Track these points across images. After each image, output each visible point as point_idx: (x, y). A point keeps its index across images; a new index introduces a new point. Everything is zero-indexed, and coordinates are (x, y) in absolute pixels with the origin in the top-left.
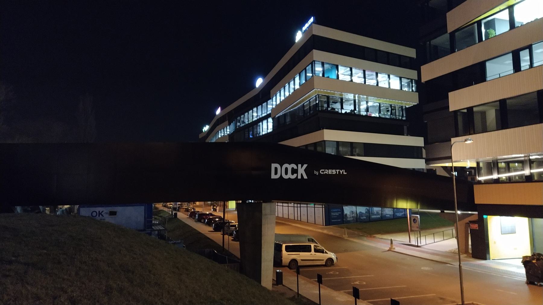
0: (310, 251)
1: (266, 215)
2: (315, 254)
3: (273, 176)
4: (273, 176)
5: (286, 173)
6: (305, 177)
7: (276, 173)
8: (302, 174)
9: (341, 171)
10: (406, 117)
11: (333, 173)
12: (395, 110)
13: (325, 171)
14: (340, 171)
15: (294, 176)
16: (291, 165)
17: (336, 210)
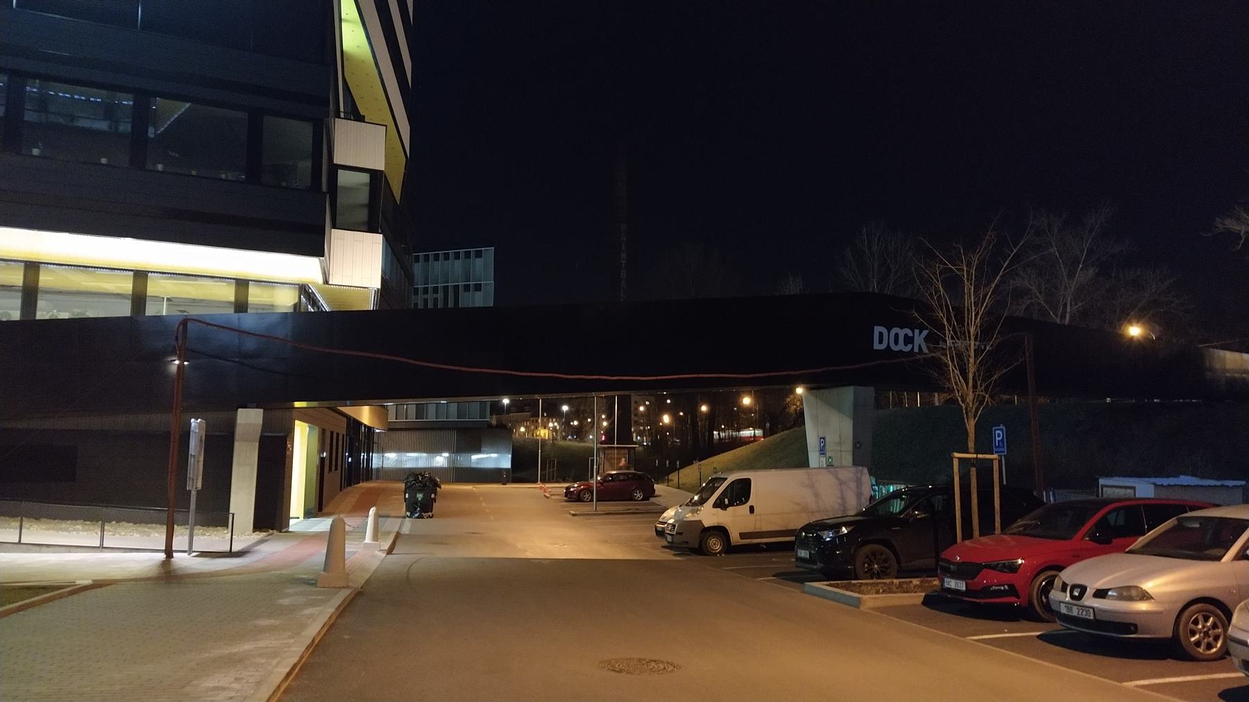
1: (9, 524)
3: (877, 346)
4: (877, 346)
5: (896, 343)
7: (881, 342)
8: (920, 346)
10: (952, 458)
12: (1061, 604)
16: (904, 330)
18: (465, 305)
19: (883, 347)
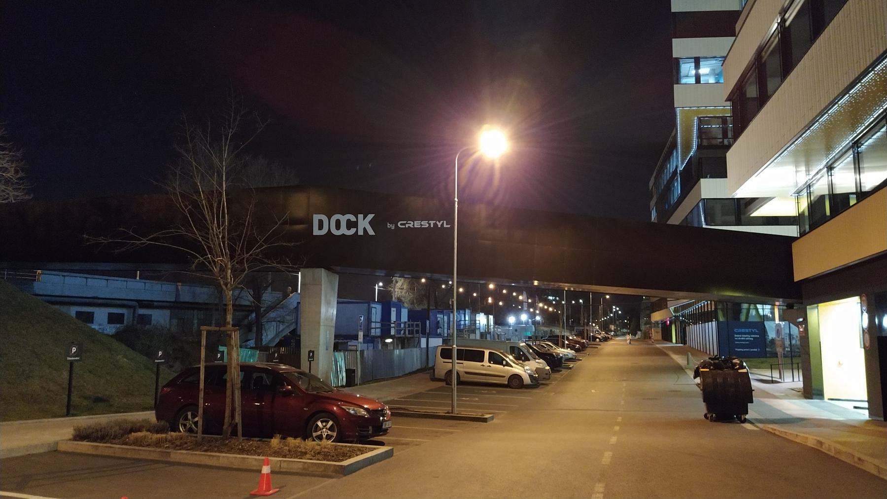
0: (482, 360)
2: (490, 366)
3: (316, 232)
4: (316, 232)
5: (338, 226)
6: (371, 232)
7: (321, 227)
8: (365, 229)
9: (439, 222)
11: (423, 226)
13: (407, 223)
14: (437, 222)
15: (353, 231)
17: (747, 330)
18: (865, 191)
19: (324, 232)
